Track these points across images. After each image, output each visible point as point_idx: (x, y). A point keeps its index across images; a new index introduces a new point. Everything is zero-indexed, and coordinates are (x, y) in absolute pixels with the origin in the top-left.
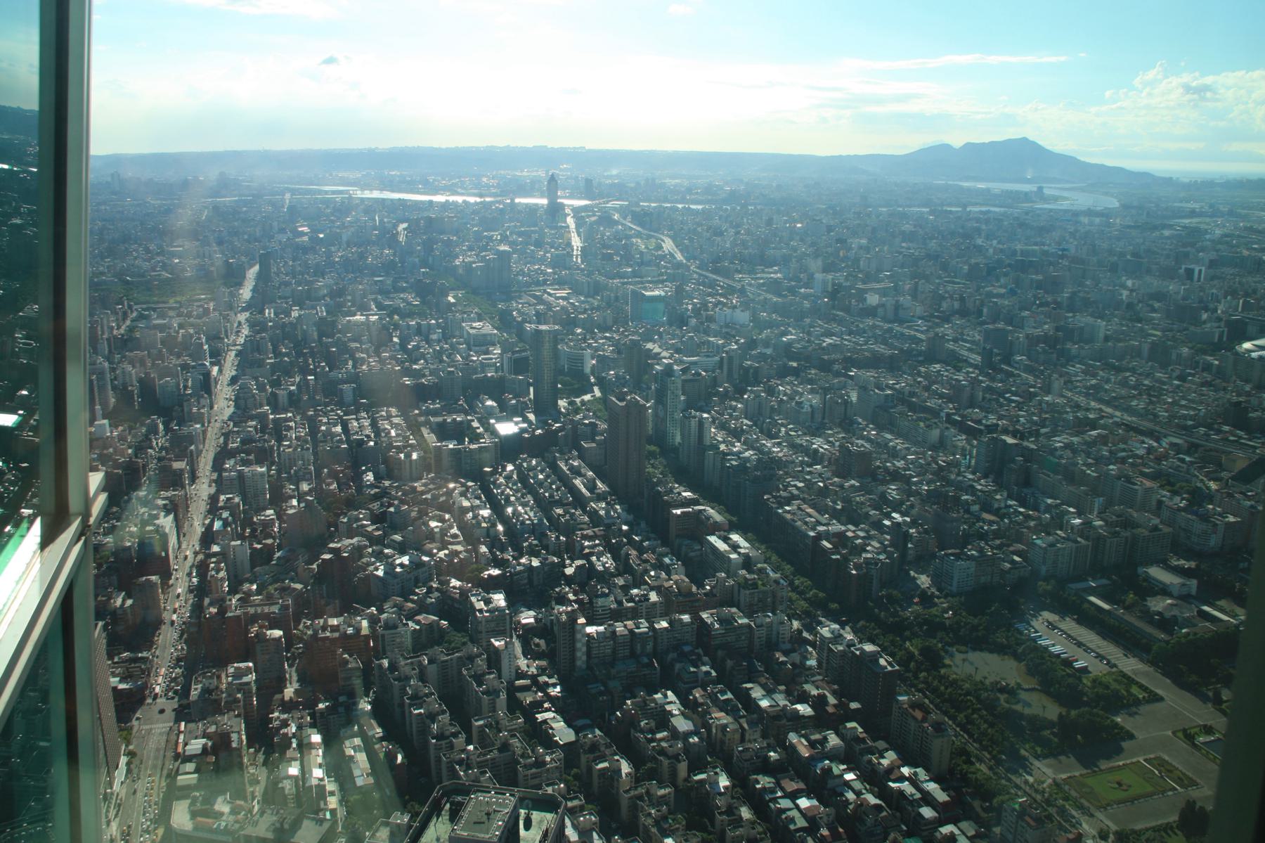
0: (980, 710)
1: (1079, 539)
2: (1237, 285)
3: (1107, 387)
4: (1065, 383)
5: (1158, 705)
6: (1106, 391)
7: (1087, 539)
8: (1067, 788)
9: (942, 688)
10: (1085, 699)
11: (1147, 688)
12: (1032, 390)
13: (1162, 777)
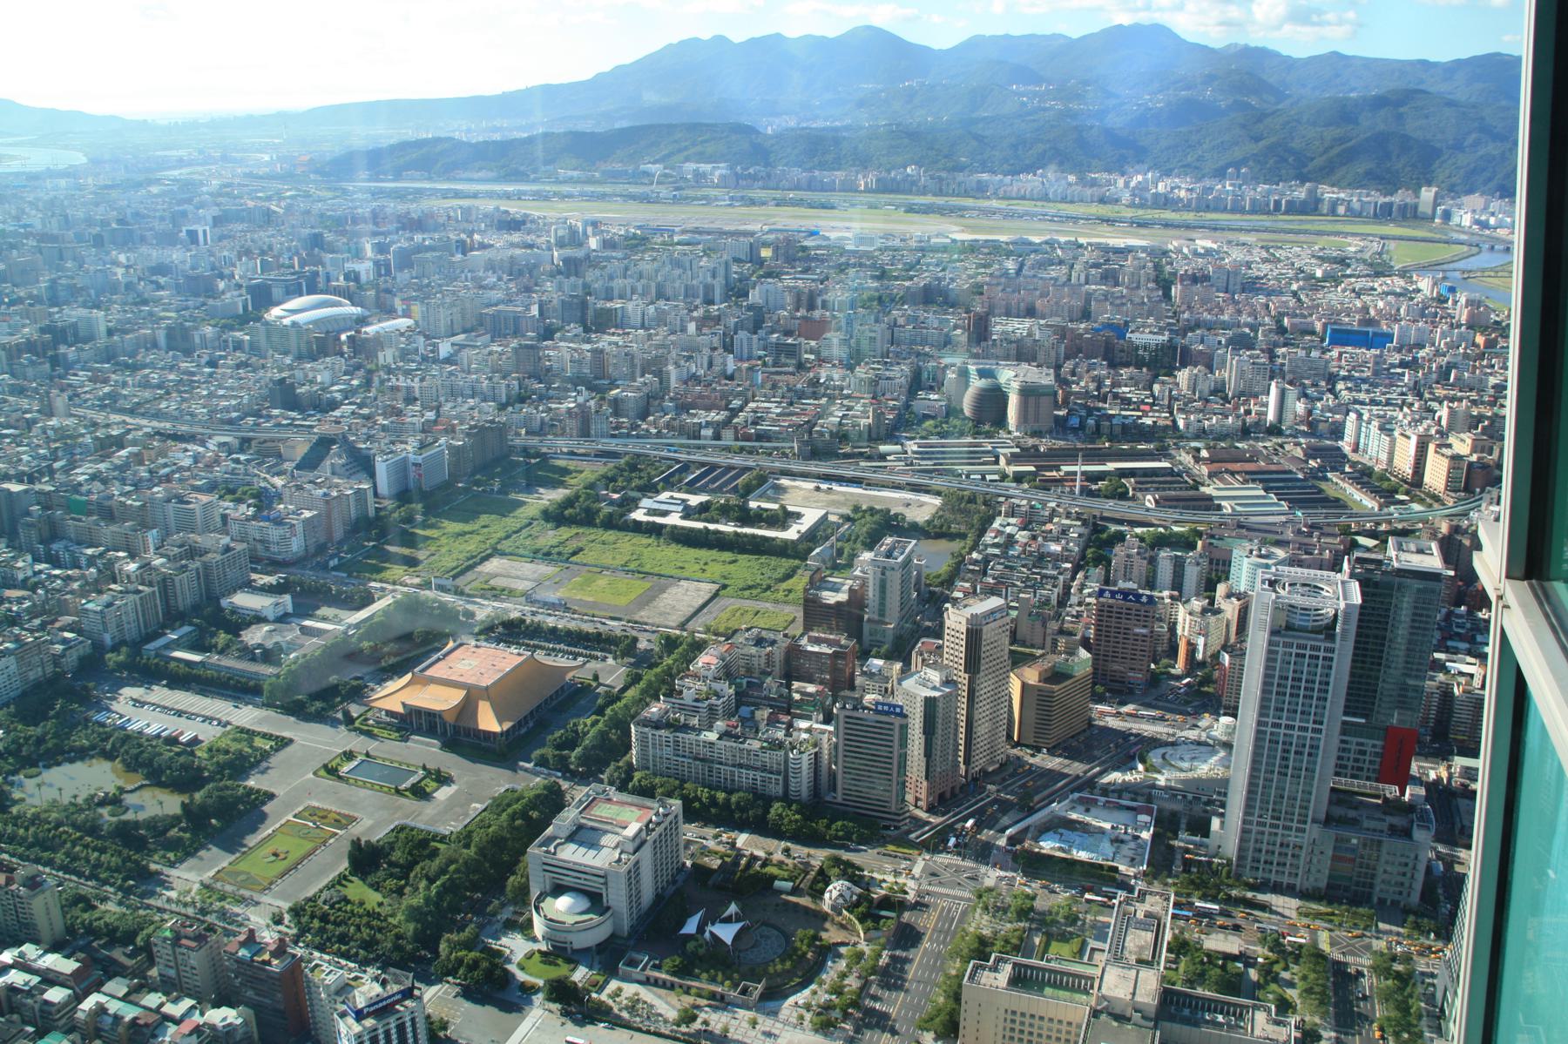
0: (81, 838)
1: (140, 588)
2: (249, 243)
3: (125, 392)
4: (70, 399)
5: (289, 749)
6: (125, 397)
7: (150, 584)
8: (219, 885)
9: (21, 831)
10: (206, 774)
11: (271, 735)
12: (28, 416)
13: (318, 827)
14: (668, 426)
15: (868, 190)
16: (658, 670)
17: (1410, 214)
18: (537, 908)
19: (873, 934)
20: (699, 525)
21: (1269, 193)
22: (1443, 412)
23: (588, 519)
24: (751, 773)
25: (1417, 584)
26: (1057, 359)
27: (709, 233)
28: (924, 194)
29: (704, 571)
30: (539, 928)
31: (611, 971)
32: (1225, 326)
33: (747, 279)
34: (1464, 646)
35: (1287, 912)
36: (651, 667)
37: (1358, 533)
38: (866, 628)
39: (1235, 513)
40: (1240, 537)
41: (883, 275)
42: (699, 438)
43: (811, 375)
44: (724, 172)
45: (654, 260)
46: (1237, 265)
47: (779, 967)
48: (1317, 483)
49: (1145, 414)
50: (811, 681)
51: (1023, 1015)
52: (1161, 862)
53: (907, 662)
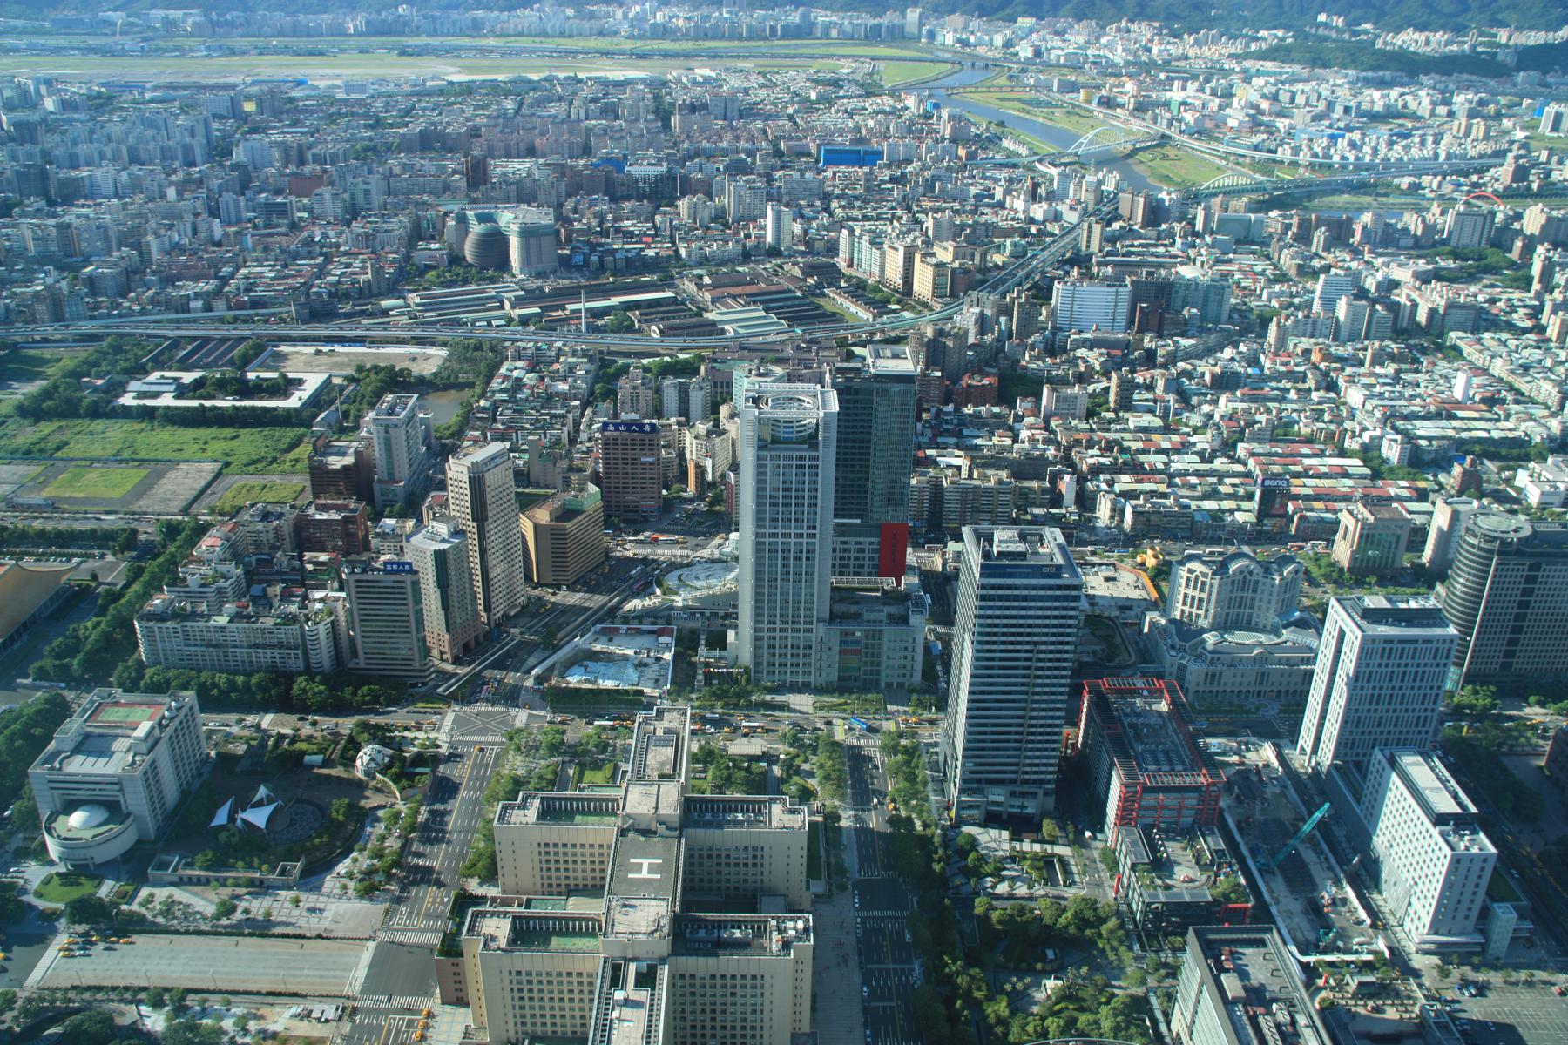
14: (152, 301)
15: (358, 34)
16: (161, 560)
17: (897, 35)
18: (49, 830)
19: (409, 792)
20: (195, 403)
21: (765, 19)
22: (929, 224)
23: (70, 410)
24: (269, 651)
25: (896, 388)
26: (559, 197)
27: (185, 88)
28: (418, 35)
29: (204, 450)
30: (54, 850)
31: (140, 879)
32: (724, 152)
33: (231, 136)
34: (952, 440)
35: (804, 709)
36: (155, 557)
37: (854, 345)
38: (377, 488)
39: (737, 336)
40: (742, 358)
41: (377, 123)
42: (188, 311)
43: (305, 234)
44: (198, 19)
45: (125, 120)
46: (733, 94)
47: (317, 841)
48: (815, 300)
49: (648, 246)
50: (323, 550)
51: (556, 845)
52: (683, 678)
53: (420, 521)
